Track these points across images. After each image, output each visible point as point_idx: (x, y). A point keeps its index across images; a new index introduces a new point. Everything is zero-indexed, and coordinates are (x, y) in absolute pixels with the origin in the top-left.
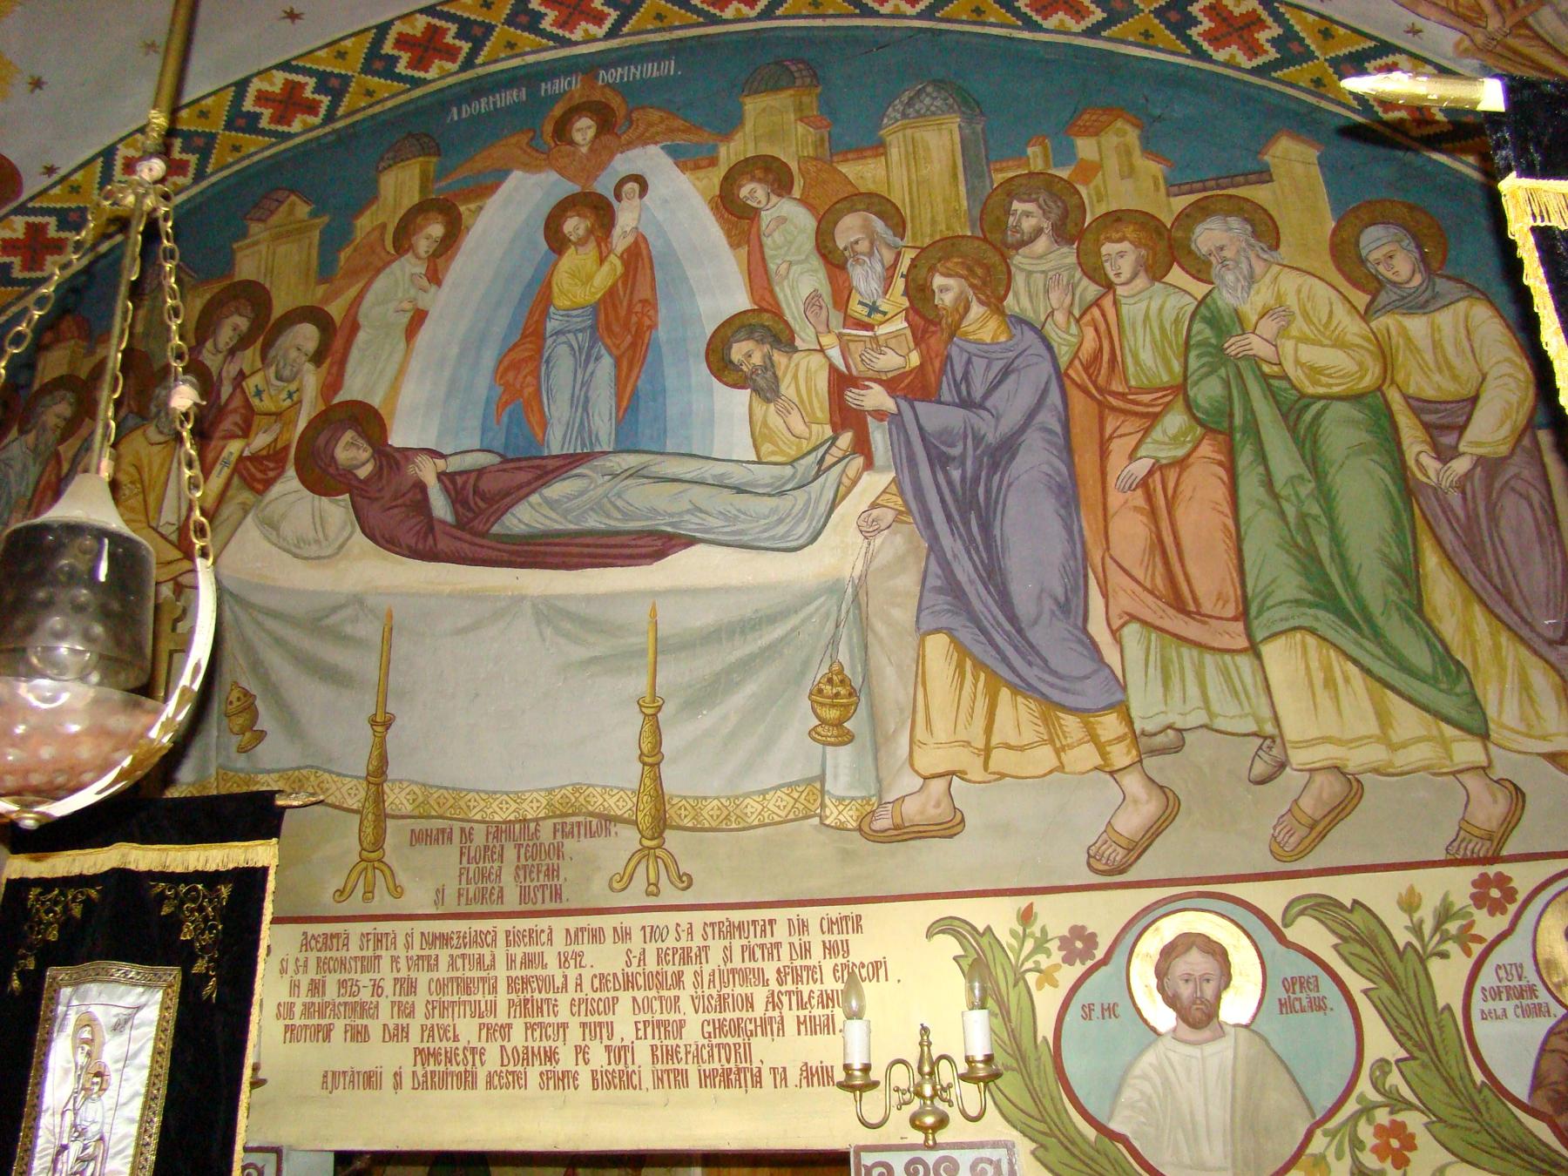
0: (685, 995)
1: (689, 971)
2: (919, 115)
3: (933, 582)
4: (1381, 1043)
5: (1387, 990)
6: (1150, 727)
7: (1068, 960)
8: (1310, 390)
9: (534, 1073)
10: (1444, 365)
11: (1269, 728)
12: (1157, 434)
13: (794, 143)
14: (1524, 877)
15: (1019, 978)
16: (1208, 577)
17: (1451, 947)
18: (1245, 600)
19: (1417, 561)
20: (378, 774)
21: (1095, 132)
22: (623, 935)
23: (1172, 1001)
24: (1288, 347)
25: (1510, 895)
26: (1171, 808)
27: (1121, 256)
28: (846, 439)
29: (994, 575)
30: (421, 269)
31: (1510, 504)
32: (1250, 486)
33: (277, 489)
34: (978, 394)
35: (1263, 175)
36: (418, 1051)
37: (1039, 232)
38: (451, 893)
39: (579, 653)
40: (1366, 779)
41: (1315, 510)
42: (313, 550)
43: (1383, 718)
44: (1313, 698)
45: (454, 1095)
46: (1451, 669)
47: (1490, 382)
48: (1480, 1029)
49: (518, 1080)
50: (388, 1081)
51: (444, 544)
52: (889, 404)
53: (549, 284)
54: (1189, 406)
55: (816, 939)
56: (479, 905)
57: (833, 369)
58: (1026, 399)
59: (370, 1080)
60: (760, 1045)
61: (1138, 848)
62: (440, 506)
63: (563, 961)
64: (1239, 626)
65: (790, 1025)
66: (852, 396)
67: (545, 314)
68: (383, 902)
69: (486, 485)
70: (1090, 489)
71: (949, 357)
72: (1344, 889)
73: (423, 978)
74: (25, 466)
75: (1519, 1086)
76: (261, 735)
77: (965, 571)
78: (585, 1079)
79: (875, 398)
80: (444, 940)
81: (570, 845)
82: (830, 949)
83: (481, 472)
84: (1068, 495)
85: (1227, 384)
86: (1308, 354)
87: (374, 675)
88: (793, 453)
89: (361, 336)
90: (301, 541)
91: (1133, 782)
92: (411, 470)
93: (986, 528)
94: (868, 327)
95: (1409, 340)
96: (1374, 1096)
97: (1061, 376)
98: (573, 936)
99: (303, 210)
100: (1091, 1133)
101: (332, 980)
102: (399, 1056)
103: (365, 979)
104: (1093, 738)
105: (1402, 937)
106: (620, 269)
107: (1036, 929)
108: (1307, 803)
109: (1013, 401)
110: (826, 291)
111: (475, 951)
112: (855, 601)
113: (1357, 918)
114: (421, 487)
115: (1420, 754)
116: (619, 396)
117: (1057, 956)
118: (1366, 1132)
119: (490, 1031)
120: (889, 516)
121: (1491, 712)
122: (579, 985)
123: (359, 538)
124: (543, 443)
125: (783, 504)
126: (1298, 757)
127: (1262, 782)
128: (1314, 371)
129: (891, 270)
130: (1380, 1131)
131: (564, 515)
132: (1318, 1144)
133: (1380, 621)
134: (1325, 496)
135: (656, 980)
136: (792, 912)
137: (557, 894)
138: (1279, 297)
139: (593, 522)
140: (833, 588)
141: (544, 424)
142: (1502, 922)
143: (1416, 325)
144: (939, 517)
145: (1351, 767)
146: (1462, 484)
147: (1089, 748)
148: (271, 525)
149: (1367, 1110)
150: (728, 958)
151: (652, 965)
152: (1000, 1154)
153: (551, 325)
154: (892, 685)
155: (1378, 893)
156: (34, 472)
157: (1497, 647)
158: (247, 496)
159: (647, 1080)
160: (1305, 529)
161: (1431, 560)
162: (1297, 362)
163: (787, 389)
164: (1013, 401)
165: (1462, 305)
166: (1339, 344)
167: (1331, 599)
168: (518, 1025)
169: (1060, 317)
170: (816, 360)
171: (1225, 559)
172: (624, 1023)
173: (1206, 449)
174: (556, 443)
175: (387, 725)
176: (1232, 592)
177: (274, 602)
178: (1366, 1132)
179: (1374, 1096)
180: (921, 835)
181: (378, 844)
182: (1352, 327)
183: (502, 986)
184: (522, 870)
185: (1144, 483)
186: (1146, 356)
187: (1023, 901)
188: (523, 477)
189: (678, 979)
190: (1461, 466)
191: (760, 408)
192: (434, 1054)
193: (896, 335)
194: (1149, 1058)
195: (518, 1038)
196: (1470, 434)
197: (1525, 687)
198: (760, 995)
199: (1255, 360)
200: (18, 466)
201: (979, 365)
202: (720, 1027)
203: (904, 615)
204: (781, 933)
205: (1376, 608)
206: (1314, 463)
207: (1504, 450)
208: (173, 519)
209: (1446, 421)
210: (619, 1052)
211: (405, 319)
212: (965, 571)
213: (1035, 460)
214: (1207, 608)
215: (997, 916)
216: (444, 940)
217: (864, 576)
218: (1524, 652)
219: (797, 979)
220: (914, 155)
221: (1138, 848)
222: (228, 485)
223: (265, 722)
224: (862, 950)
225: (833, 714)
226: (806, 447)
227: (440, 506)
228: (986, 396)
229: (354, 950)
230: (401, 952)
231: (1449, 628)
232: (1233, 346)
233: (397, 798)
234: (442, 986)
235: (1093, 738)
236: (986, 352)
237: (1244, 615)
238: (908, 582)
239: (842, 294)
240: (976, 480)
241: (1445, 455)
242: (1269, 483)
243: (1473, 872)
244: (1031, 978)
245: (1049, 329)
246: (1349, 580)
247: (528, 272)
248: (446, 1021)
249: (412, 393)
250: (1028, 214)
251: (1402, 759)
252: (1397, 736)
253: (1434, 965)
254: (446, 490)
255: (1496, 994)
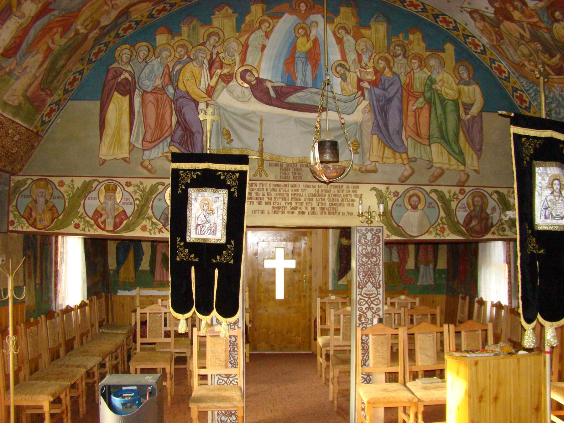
0: (326, 198)
1: (327, 194)
2: (378, 21)
3: (375, 125)
4: (442, 214)
5: (444, 206)
6: (411, 157)
7: (394, 196)
8: (446, 98)
9: (297, 211)
10: (469, 97)
11: (431, 160)
12: (418, 102)
13: (351, 22)
14: (467, 189)
15: (386, 199)
16: (424, 131)
17: (455, 200)
18: (429, 136)
19: (459, 133)
20: (261, 151)
21: (413, 34)
22: (314, 187)
23: (411, 205)
24: (443, 88)
25: (465, 192)
26: (413, 172)
27: (415, 63)
28: (360, 93)
29: (386, 125)
30: (263, 34)
31: (475, 125)
32: (433, 115)
33: (231, 84)
34: (386, 87)
35: (443, 51)
36: (273, 207)
37: (400, 54)
38: (279, 176)
39: (304, 130)
40: (445, 170)
41: (443, 121)
42: (242, 99)
43: (449, 160)
44: (438, 155)
45: (280, 215)
46: (461, 153)
47: (476, 101)
48: (457, 213)
49: (293, 213)
50: (266, 212)
51: (274, 103)
52: (369, 87)
53: (296, 45)
54: (424, 97)
55: (351, 189)
56: (285, 179)
57: (358, 77)
58: (395, 90)
59: (263, 212)
60: (340, 208)
61: (407, 178)
62: (272, 93)
63: (302, 191)
64: (428, 141)
65: (346, 205)
66: (361, 84)
67: (295, 53)
68: (264, 177)
69: (283, 90)
70: (404, 111)
71: (381, 79)
72: (439, 188)
73: (273, 193)
74: (159, 67)
75: (461, 222)
76: (232, 140)
77: (381, 123)
78: (307, 213)
79: (366, 85)
80: (278, 186)
81: (303, 169)
82: (353, 191)
83: (282, 87)
84: (401, 111)
85: (431, 93)
86: (447, 90)
87: (259, 129)
88: (349, 94)
89: (250, 49)
90: (238, 97)
91: (407, 167)
92: (265, 84)
93: (386, 115)
94: (365, 69)
95: (464, 91)
96: (440, 222)
97: (402, 87)
98: (304, 186)
99: (230, 11)
100: (396, 225)
101: (253, 193)
102: (269, 207)
103: (261, 192)
104: (401, 158)
105: (448, 197)
106: (312, 45)
107: (389, 191)
108: (435, 174)
109: (392, 90)
110: (357, 59)
111: (284, 188)
112: (360, 126)
113: (441, 194)
114: (268, 89)
115: (455, 167)
116: (313, 74)
117: (392, 196)
118: (438, 228)
119: (288, 203)
120: (368, 110)
121: (466, 161)
122: (306, 195)
123: (253, 99)
124: (295, 83)
125: (347, 104)
126: (435, 165)
127: (428, 169)
128: (447, 94)
129: (370, 57)
130: (441, 228)
131: (301, 100)
132: (431, 229)
133: (451, 143)
134: (445, 119)
135: (321, 195)
136: (347, 184)
137: (301, 178)
138: (443, 78)
139: (307, 102)
140: (356, 123)
141: (296, 79)
142: (463, 196)
143: (466, 88)
144: (388, 140)
145: (443, 168)
146: (468, 120)
147: (400, 160)
148: (231, 92)
149: (439, 224)
150: (334, 192)
151: (320, 192)
152: (381, 228)
153: (297, 55)
154: (366, 144)
155: (445, 190)
156: (162, 69)
157: (469, 150)
158: (223, 84)
159: (319, 213)
160: (441, 124)
161: (461, 133)
162: (445, 92)
163: (348, 80)
164: (392, 90)
165: (474, 86)
166: (452, 89)
167: (444, 138)
168: (293, 203)
169: (403, 74)
170: (354, 75)
171: (427, 128)
172: (314, 203)
173: (426, 106)
174: (299, 83)
175: (263, 140)
176: (427, 134)
177: (232, 110)
178: (438, 228)
179: (440, 222)
180: (370, 172)
181: (262, 165)
182: (454, 86)
183: (290, 195)
184: (294, 173)
185: (415, 111)
186: (418, 85)
187: (387, 186)
188: (292, 90)
189: (325, 195)
190: (469, 116)
191: (343, 83)
192: (276, 208)
193: (371, 72)
194: (406, 214)
195: (293, 205)
196: (471, 111)
197: (472, 157)
198: (340, 199)
199: (437, 90)
200: (156, 67)
201: (387, 82)
202: (333, 204)
203: (369, 130)
204: (344, 188)
205: (451, 140)
206: (445, 113)
207: (476, 115)
208: (204, 87)
209: (468, 107)
210: (313, 208)
211: (261, 46)
212: (381, 123)
213: (396, 102)
214: (423, 136)
215: (382, 188)
216: (278, 186)
217: (362, 122)
218: (473, 152)
219: (347, 197)
220: (377, 31)
221: (407, 178)
222: (218, 80)
223: (232, 137)
224: (359, 192)
225: (355, 148)
226: (352, 93)
227: (272, 93)
228: (388, 88)
229: (258, 187)
230: (268, 187)
231: (462, 146)
232: (434, 86)
233: (266, 156)
234: (277, 194)
235: (401, 158)
236: (389, 79)
237: (429, 139)
238: (370, 124)
239: (360, 60)
240: (384, 105)
241: (466, 114)
242: (436, 113)
243: (459, 188)
244: (388, 199)
245: (400, 76)
246: (447, 134)
247: (291, 41)
248: (279, 201)
249: (264, 66)
250: (398, 50)
251: (451, 168)
252: (451, 163)
253: (452, 203)
254: (273, 90)
255: (460, 208)
